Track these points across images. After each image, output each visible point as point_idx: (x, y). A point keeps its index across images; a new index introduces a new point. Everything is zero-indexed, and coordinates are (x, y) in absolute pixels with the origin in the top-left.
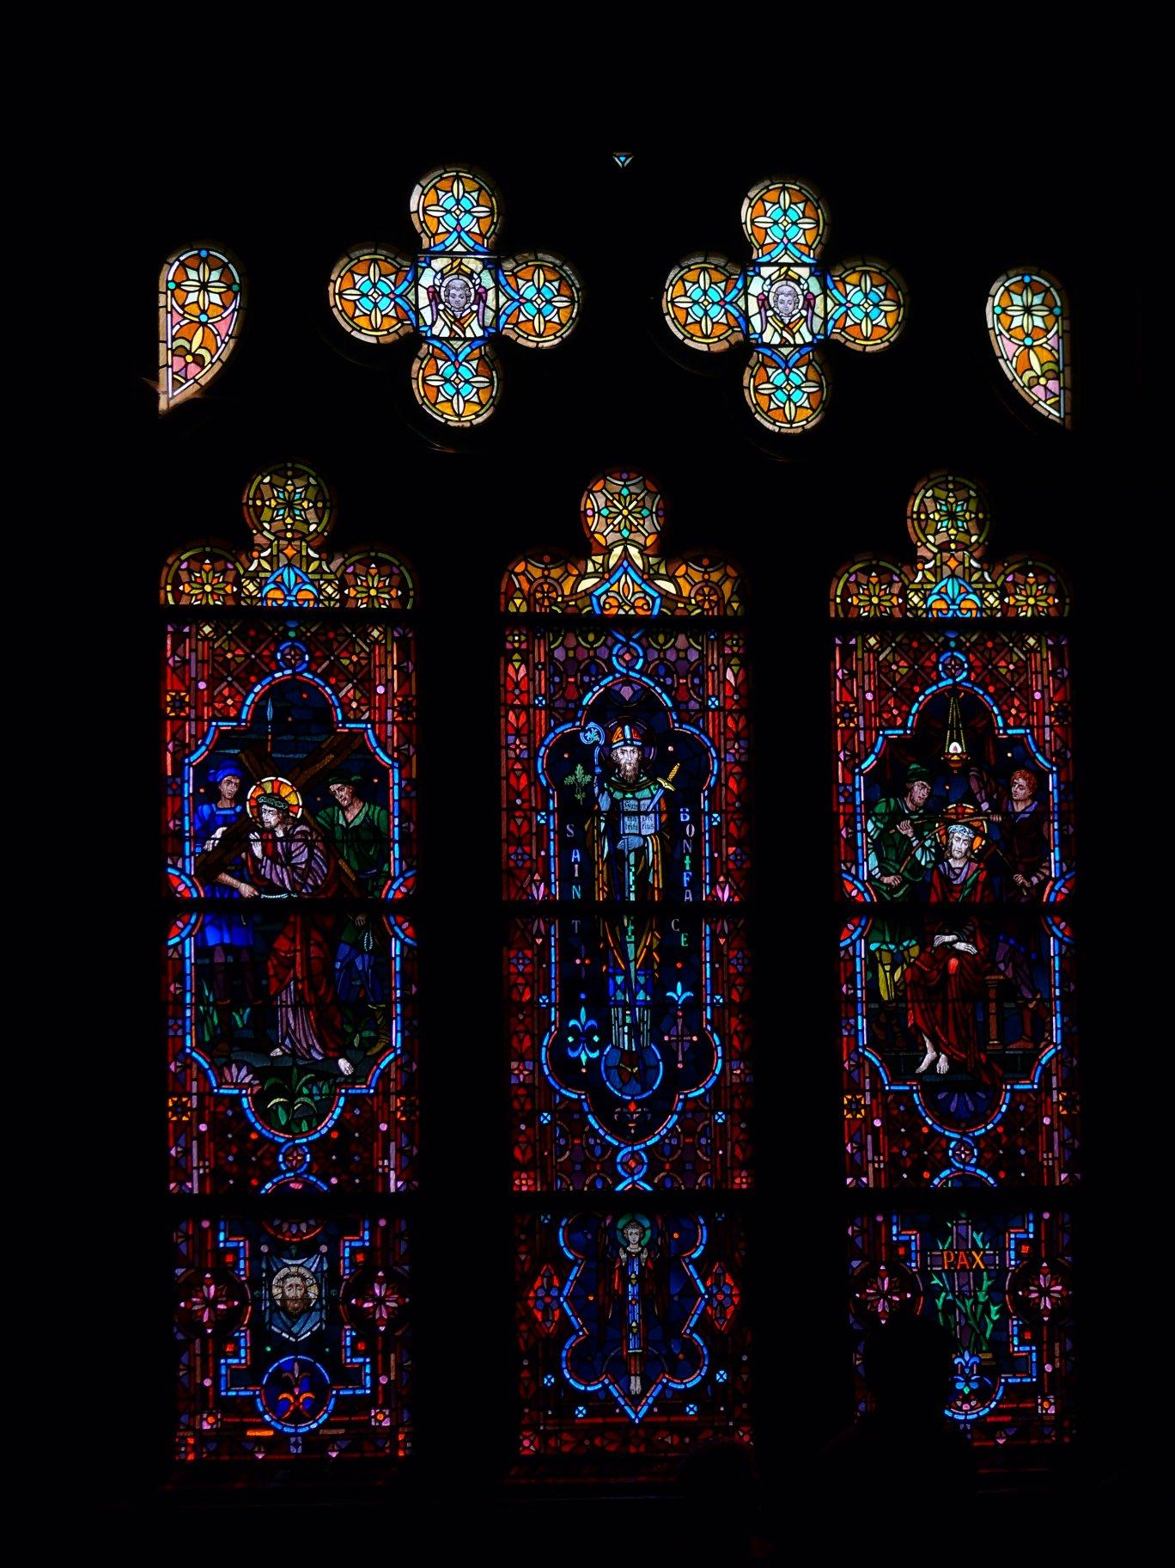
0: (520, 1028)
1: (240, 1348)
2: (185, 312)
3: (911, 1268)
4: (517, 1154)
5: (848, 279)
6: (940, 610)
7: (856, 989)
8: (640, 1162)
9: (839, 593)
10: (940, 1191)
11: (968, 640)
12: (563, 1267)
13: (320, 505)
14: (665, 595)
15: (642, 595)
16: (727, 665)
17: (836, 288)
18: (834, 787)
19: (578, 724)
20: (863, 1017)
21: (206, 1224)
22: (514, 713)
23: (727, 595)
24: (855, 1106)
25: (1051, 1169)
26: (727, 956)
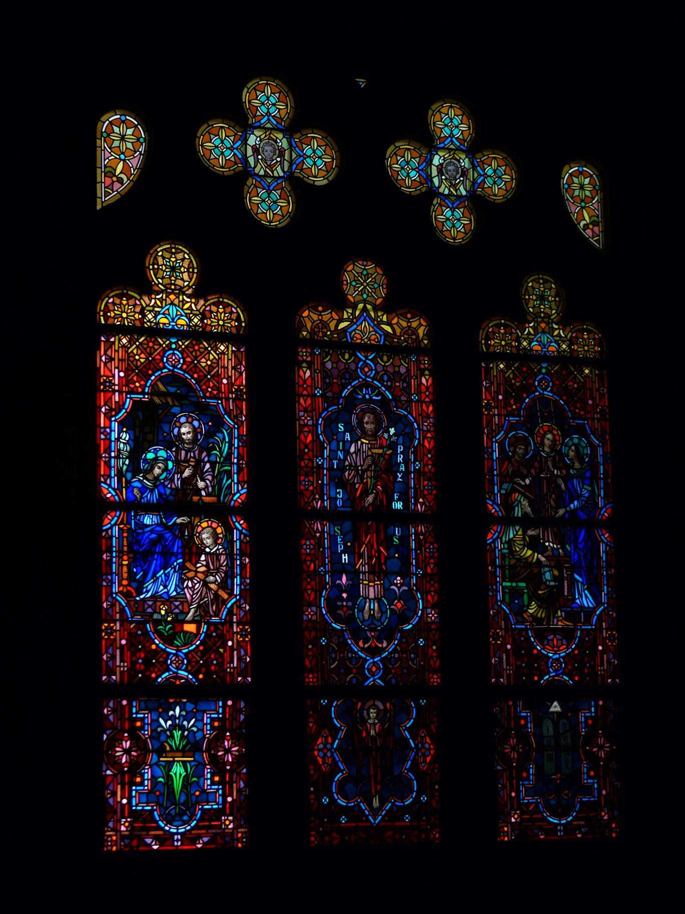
0: (309, 587)
2: (112, 151)
4: (307, 663)
6: (164, 324)
8: (378, 668)
11: (183, 344)
12: (335, 731)
14: (386, 334)
16: (423, 375)
18: (98, 429)
22: (304, 399)
23: (421, 335)
25: (602, 676)
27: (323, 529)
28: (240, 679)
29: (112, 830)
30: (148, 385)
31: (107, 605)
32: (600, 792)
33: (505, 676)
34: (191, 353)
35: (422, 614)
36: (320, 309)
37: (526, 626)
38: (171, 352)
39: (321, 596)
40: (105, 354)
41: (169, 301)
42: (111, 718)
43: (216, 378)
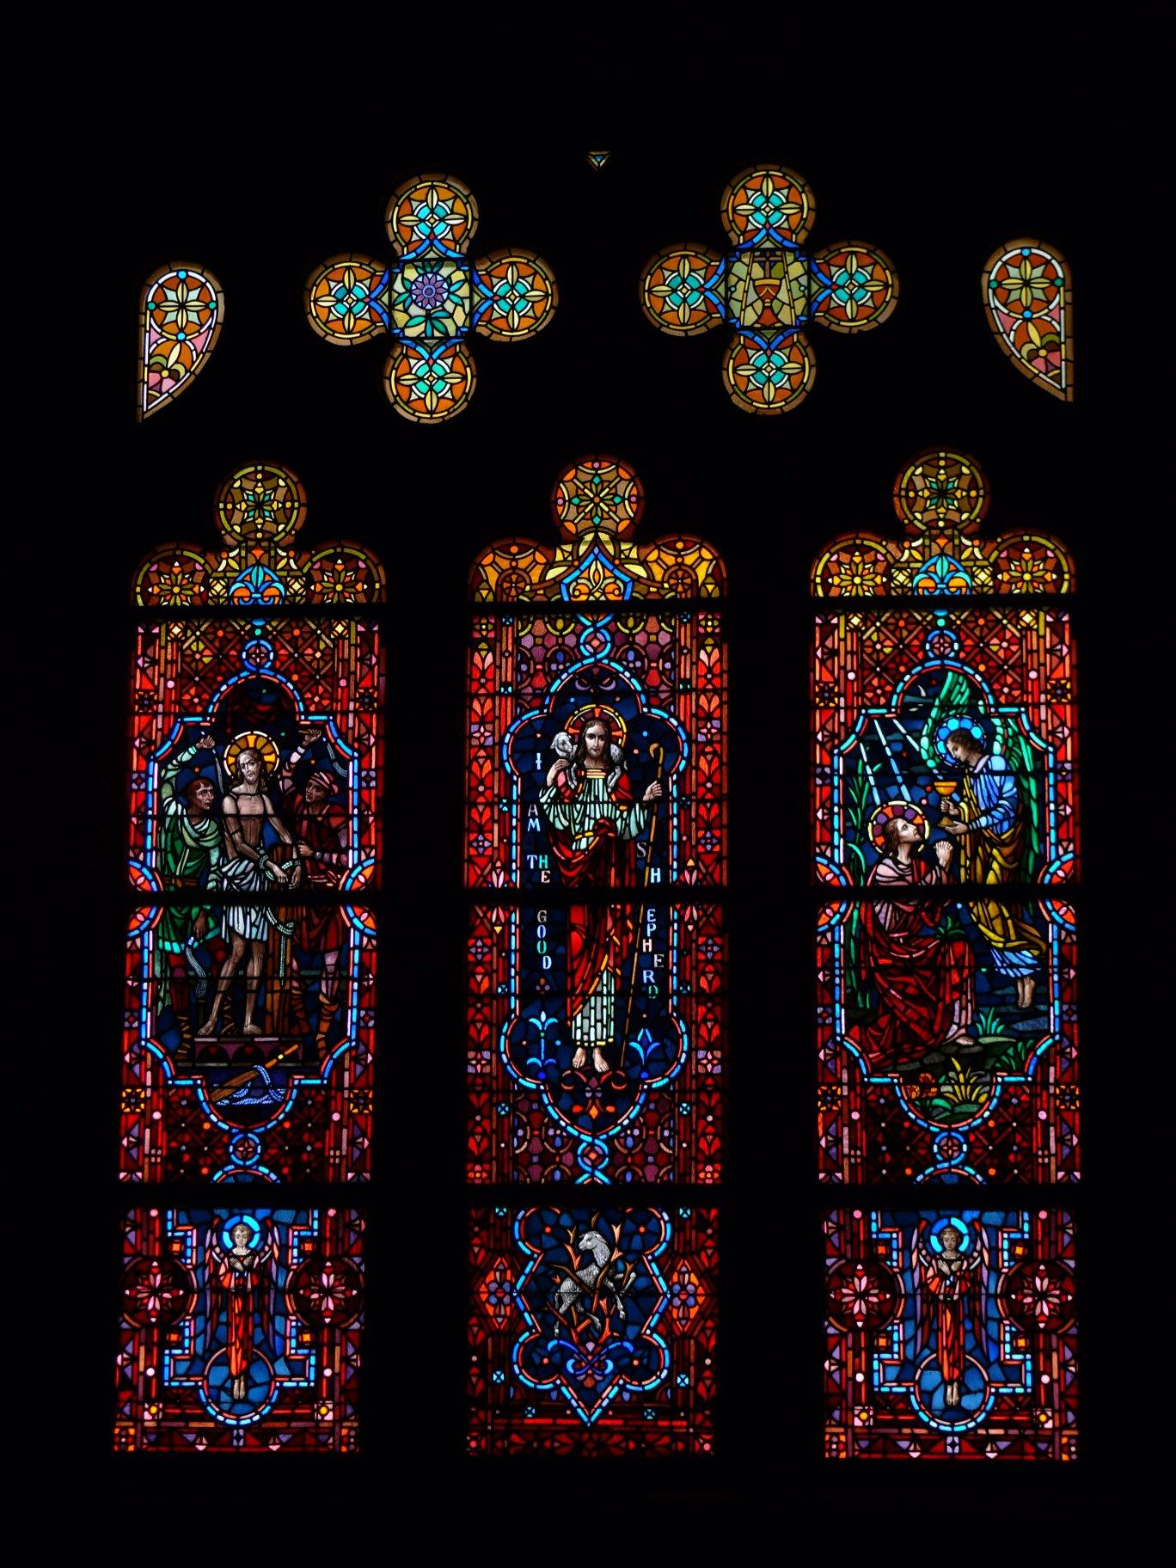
1: (184, 1338)
3: (186, 1264)
4: (472, 1145)
5: (832, 262)
10: (222, 1184)
11: (958, 618)
14: (636, 579)
15: (612, 580)
16: (702, 646)
20: (841, 1007)
21: (154, 1213)
24: (135, 1100)
26: (696, 941)
28: (350, 1175)
29: (839, 1424)
30: (898, 690)
31: (825, 1055)
32: (319, 1374)
33: (146, 1167)
34: (972, 630)
35: (688, 1059)
38: (254, 642)
39: (499, 1034)
40: (822, 645)
41: (252, 560)
42: (835, 1239)
43: (1018, 670)
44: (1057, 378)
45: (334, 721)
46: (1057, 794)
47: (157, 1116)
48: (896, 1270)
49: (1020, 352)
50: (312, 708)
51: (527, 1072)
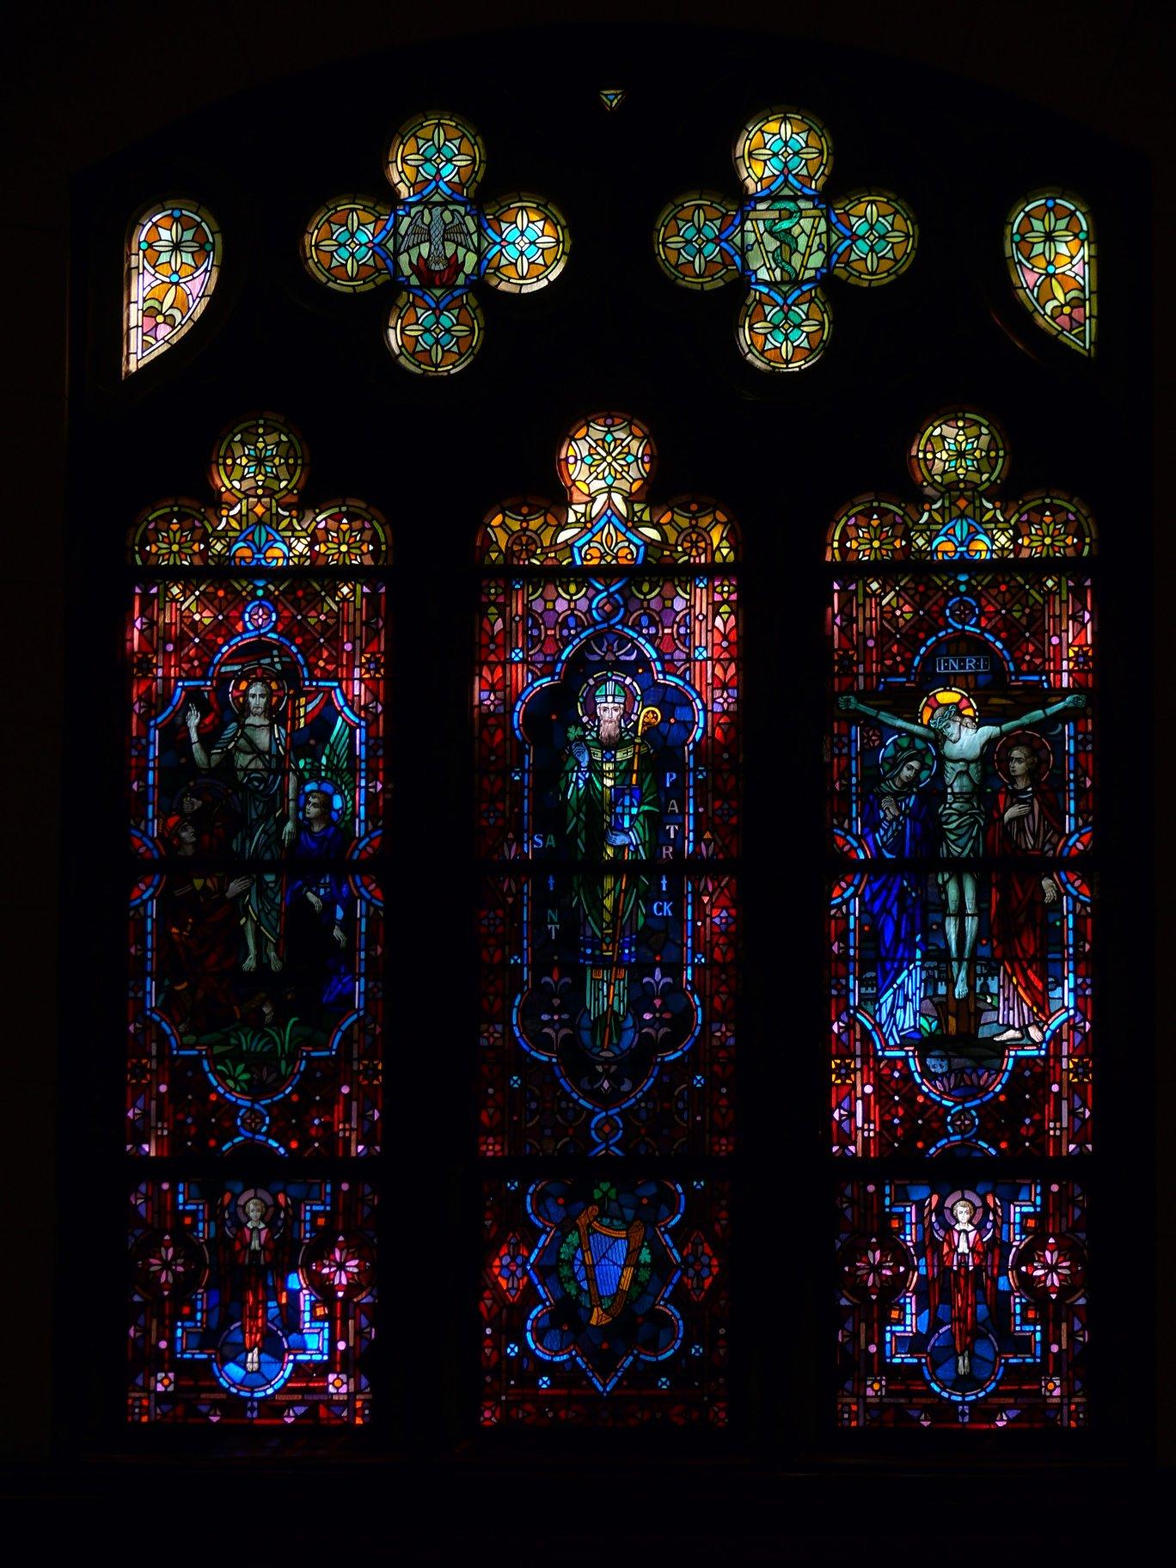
3: (197, 1237)
4: (484, 1118)
7: (848, 947)
9: (837, 537)
13: (291, 461)
14: (650, 543)
15: (626, 544)
16: (716, 613)
17: (490, 226)
19: (661, 676)
21: (165, 1186)
25: (1058, 1139)
27: (520, 891)
29: (852, 1395)
31: (839, 1027)
36: (694, 507)
37: (200, 1051)
41: (955, 512)
44: (1082, 338)
45: (340, 687)
46: (1077, 764)
47: (163, 1088)
48: (910, 1244)
49: (1043, 308)
50: (1024, 667)
51: (543, 1043)
